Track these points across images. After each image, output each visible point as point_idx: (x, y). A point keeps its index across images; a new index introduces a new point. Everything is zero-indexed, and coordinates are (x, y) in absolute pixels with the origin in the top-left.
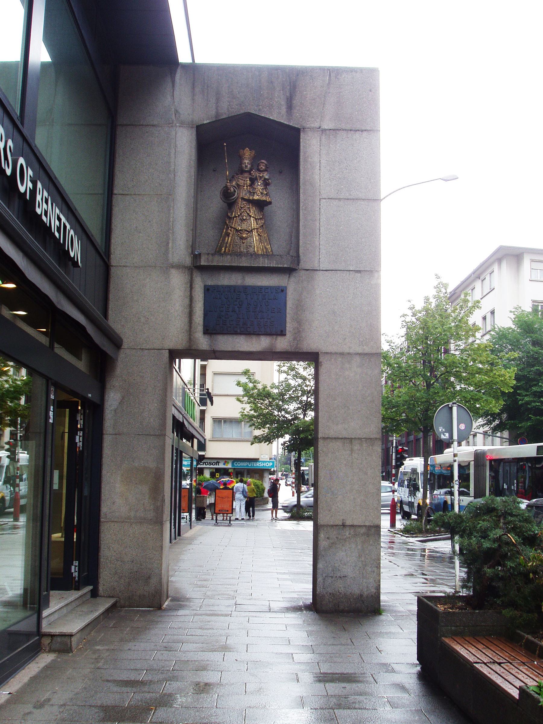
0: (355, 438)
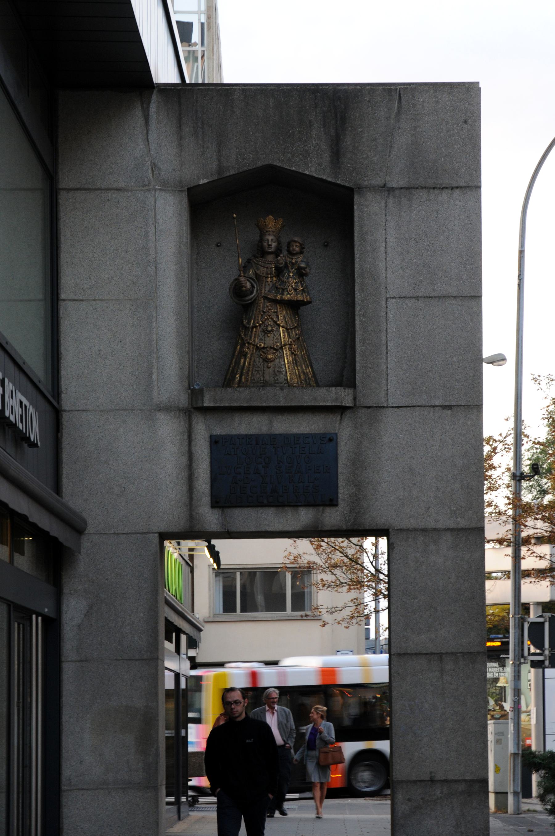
0: (447, 653)
